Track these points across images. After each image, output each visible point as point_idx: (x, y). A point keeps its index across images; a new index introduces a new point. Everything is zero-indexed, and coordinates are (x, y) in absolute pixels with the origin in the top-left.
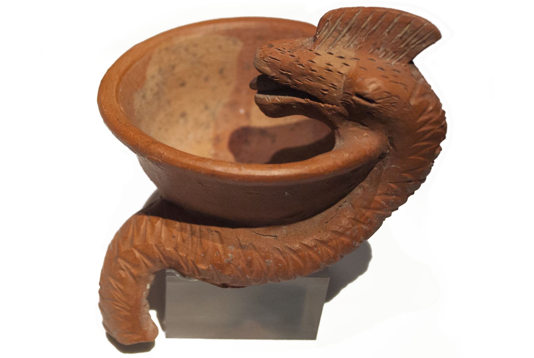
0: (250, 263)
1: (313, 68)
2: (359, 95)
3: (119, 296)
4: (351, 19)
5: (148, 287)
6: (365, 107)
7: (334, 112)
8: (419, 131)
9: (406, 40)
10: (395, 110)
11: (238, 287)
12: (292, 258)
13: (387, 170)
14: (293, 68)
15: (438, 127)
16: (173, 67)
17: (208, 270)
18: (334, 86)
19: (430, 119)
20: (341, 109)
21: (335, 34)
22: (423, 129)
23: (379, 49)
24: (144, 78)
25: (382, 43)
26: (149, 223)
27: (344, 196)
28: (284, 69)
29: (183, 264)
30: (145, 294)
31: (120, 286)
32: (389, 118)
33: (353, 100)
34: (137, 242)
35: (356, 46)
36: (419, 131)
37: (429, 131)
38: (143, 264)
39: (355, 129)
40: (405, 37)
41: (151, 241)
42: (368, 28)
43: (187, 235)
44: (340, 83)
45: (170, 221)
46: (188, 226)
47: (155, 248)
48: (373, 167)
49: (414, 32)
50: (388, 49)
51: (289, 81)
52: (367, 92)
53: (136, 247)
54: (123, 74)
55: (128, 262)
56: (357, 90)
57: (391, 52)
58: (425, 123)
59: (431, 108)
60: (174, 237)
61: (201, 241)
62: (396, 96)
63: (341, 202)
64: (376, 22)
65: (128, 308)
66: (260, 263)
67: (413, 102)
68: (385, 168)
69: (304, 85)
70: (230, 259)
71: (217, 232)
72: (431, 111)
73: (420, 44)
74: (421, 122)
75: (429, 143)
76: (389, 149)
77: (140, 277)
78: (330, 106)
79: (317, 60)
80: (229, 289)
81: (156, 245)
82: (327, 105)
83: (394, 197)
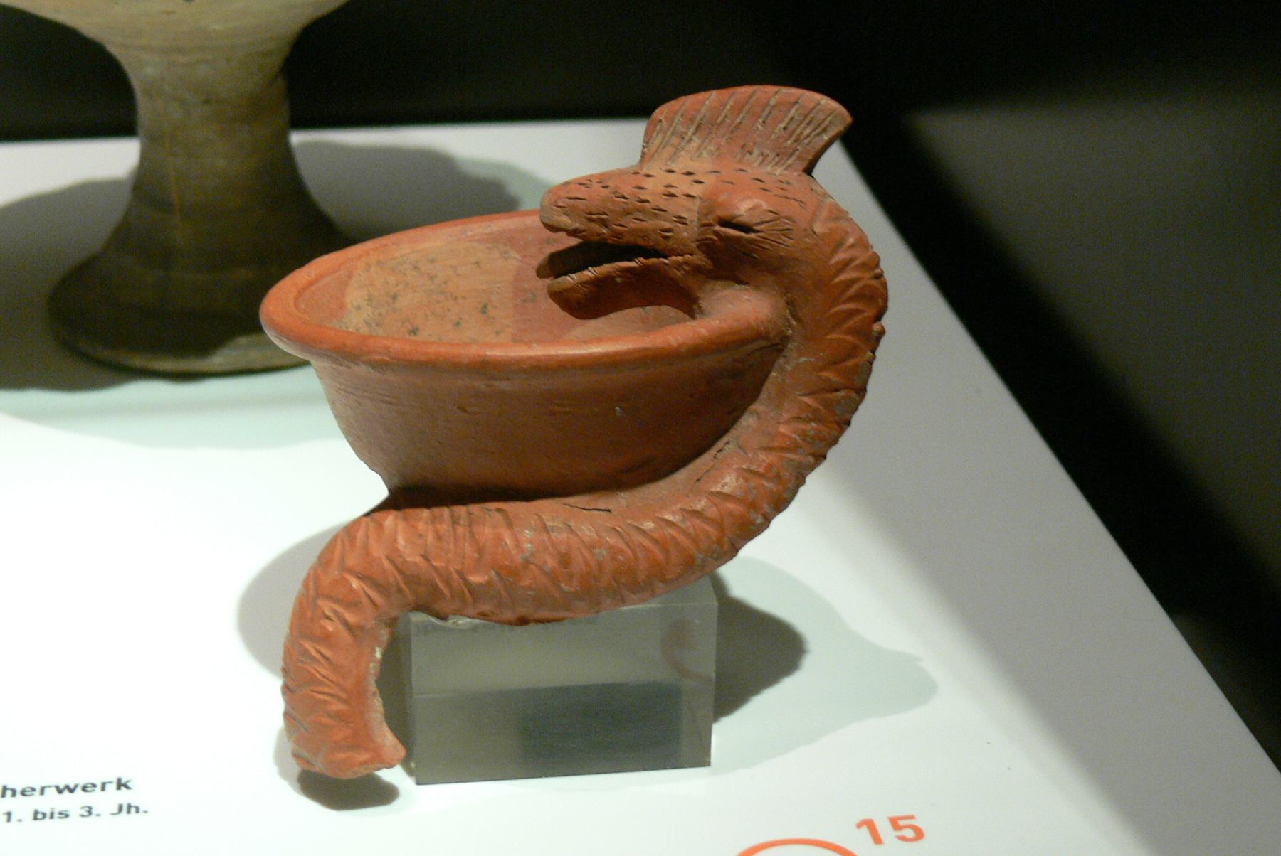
0: (565, 560)
1: (643, 197)
2: (726, 223)
3: (324, 672)
4: (698, 111)
5: (378, 655)
6: (738, 239)
7: (687, 268)
8: (837, 280)
9: (793, 132)
10: (790, 242)
11: (549, 621)
12: (641, 545)
13: (794, 369)
14: (609, 205)
15: (868, 275)
16: (394, 297)
17: (489, 583)
18: (681, 220)
19: (851, 260)
20: (699, 259)
21: (675, 140)
22: (843, 277)
23: (750, 153)
24: (342, 306)
25: (755, 143)
26: (372, 525)
27: (725, 431)
28: (593, 210)
29: (440, 585)
30: (373, 668)
31: (327, 653)
32: (781, 257)
33: (716, 233)
34: (351, 561)
35: (711, 153)
36: (837, 280)
37: (854, 281)
38: (365, 601)
39: (727, 292)
40: (792, 126)
41: (378, 551)
42: (728, 121)
43: (444, 527)
44: (691, 211)
45: (410, 512)
46: (446, 511)
47: (386, 563)
48: (769, 372)
49: (806, 117)
50: (766, 151)
51: (605, 231)
52: (737, 212)
53: (350, 571)
54: (304, 289)
55: (337, 601)
56: (721, 213)
57: (772, 155)
58: (845, 265)
59: (851, 240)
60: (421, 536)
61: (471, 532)
62: (788, 218)
63: (720, 444)
64: (740, 111)
65: (344, 695)
66: (584, 557)
67: (819, 228)
68: (789, 368)
69: (633, 231)
70: (527, 554)
71: (499, 510)
72: (852, 246)
73: (818, 134)
74: (841, 282)
75: (860, 306)
76: (790, 326)
77: (362, 628)
78: (680, 258)
79: (648, 184)
80: (532, 628)
81: (388, 558)
82: (674, 258)
83: (813, 424)
